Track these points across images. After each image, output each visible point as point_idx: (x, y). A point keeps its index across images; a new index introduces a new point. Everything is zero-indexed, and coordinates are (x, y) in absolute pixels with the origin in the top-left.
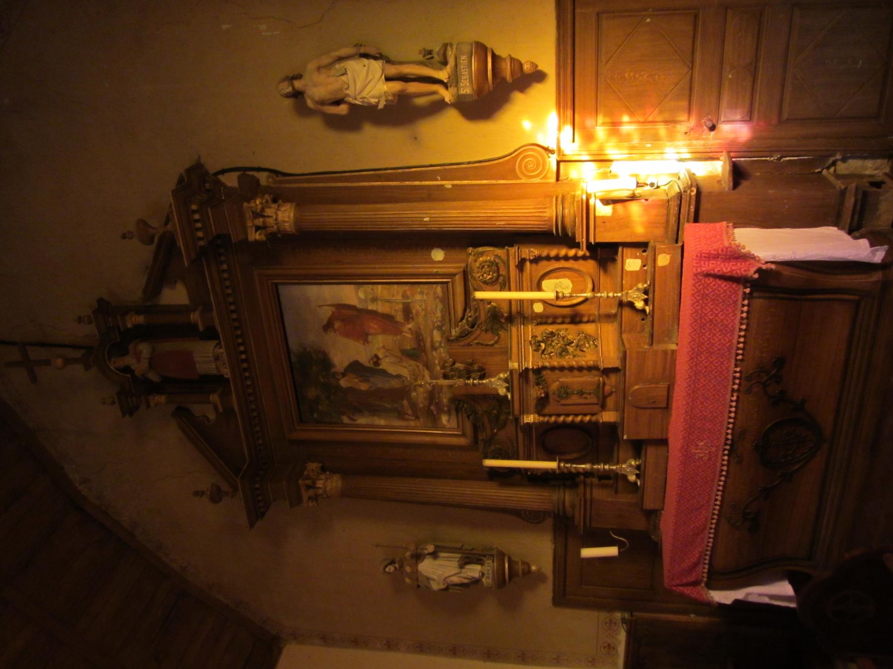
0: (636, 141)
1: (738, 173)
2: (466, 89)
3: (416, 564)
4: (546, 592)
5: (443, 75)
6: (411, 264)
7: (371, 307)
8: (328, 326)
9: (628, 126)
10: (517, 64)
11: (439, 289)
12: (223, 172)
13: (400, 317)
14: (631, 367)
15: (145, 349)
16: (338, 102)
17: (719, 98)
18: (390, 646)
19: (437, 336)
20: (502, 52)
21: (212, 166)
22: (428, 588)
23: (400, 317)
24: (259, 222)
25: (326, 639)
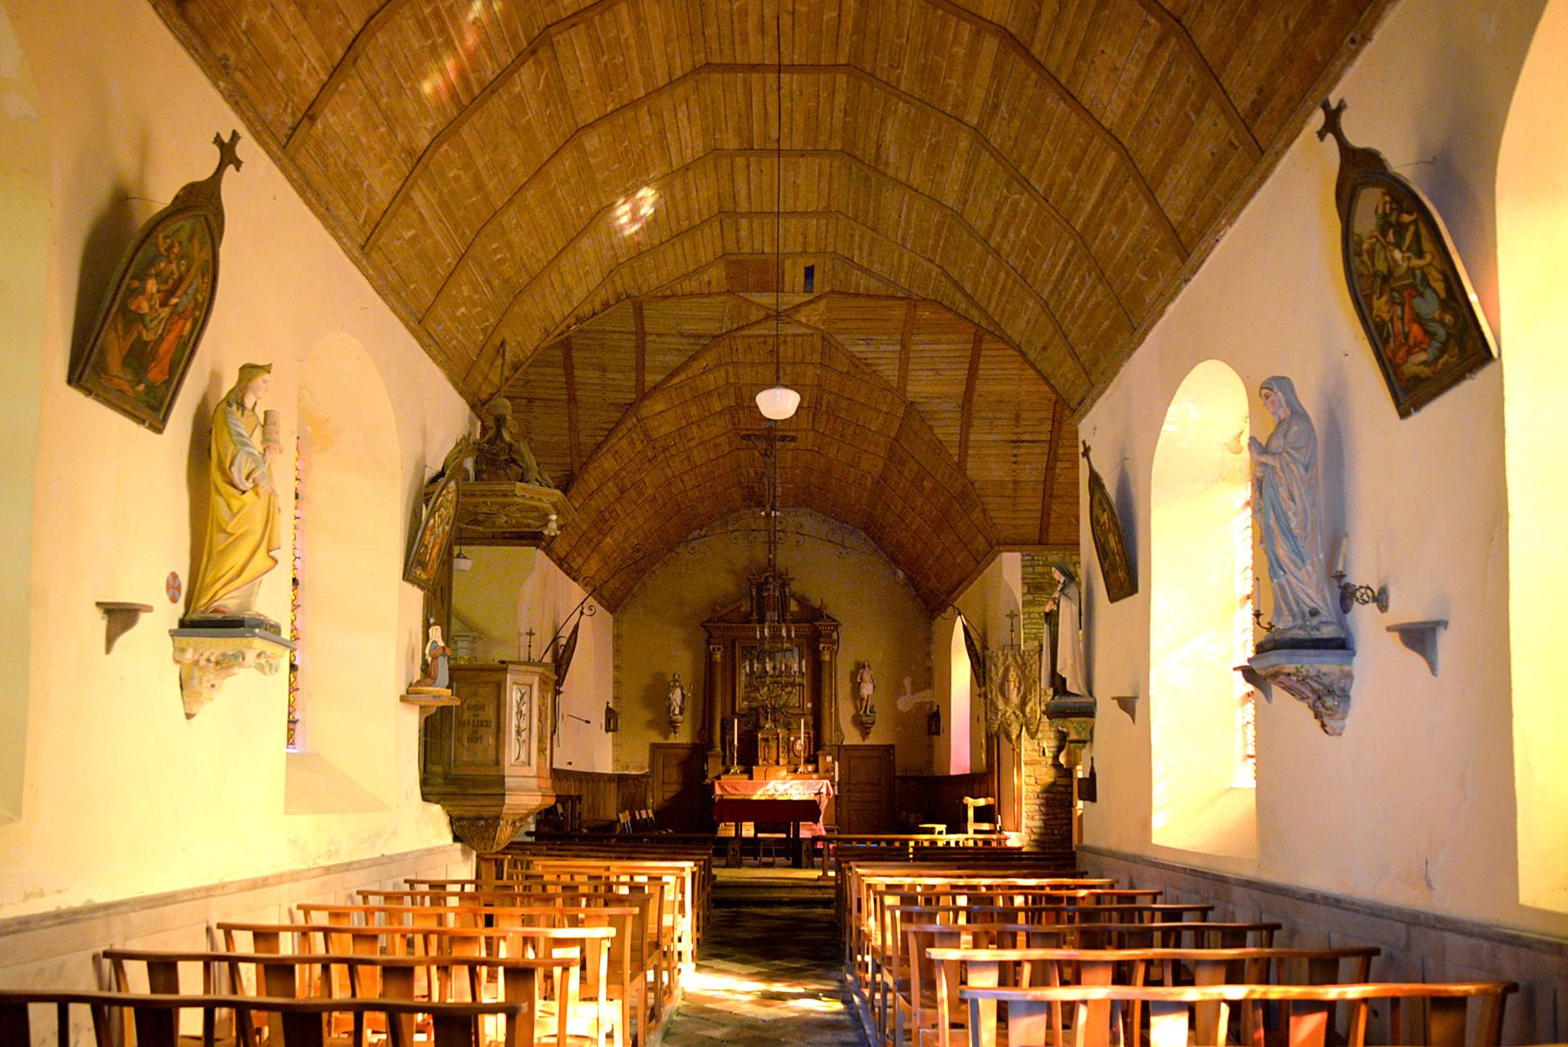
4: (659, 740)
5: (868, 712)
18: (616, 668)
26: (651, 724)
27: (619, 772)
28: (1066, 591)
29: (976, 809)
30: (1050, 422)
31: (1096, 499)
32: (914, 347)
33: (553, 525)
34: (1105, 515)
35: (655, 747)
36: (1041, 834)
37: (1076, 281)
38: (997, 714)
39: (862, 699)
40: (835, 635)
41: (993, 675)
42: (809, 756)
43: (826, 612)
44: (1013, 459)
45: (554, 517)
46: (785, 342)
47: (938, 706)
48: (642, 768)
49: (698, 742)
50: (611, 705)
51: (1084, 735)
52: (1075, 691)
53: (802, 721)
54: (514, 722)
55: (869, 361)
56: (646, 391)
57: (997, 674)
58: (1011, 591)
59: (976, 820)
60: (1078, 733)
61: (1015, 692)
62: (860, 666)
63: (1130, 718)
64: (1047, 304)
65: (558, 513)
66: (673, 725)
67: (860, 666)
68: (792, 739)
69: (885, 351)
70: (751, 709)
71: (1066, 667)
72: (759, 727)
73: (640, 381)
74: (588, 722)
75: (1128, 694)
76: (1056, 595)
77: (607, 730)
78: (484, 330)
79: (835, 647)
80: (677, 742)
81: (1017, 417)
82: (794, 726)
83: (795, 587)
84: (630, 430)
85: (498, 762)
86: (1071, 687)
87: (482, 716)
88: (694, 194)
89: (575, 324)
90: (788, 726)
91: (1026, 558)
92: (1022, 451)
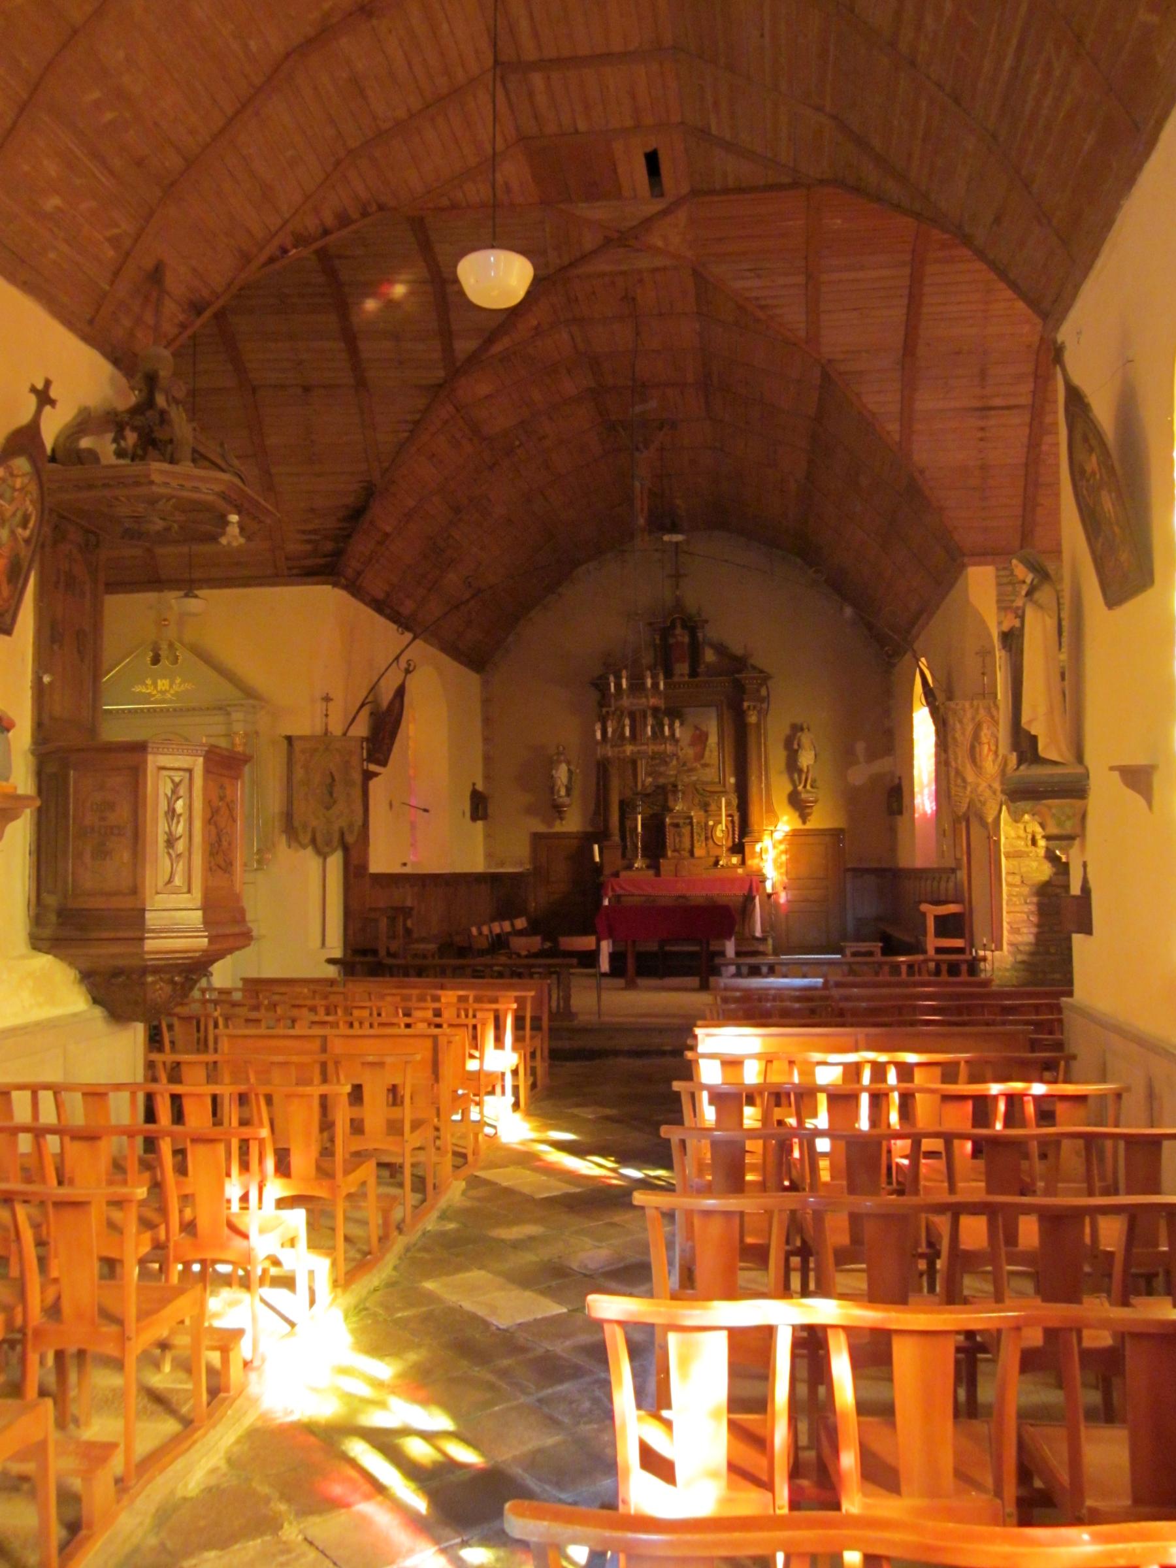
0: (779, 860)
1: (769, 896)
2: (804, 796)
3: (565, 762)
4: (542, 828)
5: (808, 787)
6: (729, 767)
7: (707, 749)
8: (696, 728)
9: (784, 858)
10: (810, 814)
11: (717, 780)
12: (767, 688)
13: (703, 762)
14: (693, 861)
15: (686, 640)
16: (799, 745)
17: (795, 889)
18: (487, 740)
19: (694, 778)
20: (814, 808)
21: (770, 683)
22: (552, 769)
23: (703, 762)
24: (752, 708)
25: (486, 702)
26: (530, 810)
27: (492, 871)
28: (1037, 595)
29: (937, 918)
30: (1031, 379)
31: (1078, 436)
32: (824, 277)
33: (233, 530)
34: (1094, 458)
35: (537, 837)
36: (1032, 954)
37: (1037, 77)
38: (965, 788)
39: (800, 771)
40: (764, 692)
41: (958, 735)
42: (734, 844)
43: (752, 661)
44: (980, 435)
45: (234, 518)
46: (641, 281)
47: (900, 778)
48: (521, 864)
49: (590, 829)
50: (480, 787)
51: (1069, 827)
52: (1053, 755)
53: (723, 800)
54: (163, 826)
55: (763, 303)
56: (458, 364)
57: (963, 734)
58: (983, 622)
59: (939, 933)
60: (1060, 824)
61: (991, 757)
62: (797, 729)
63: (1142, 802)
64: (994, 136)
65: (239, 513)
66: (558, 810)
67: (797, 729)
68: (711, 823)
69: (785, 286)
70: (658, 787)
71: (1036, 719)
72: (667, 809)
73: (448, 350)
74: (426, 810)
75: (1141, 760)
76: (1019, 603)
77: (475, 817)
78: (115, 241)
79: (765, 706)
80: (564, 829)
81: (983, 374)
82: (713, 807)
83: (711, 632)
84: (446, 422)
85: (135, 890)
86: (1043, 750)
87: (112, 818)
88: (445, 26)
89: (295, 247)
90: (705, 807)
91: (1002, 573)
92: (992, 422)
